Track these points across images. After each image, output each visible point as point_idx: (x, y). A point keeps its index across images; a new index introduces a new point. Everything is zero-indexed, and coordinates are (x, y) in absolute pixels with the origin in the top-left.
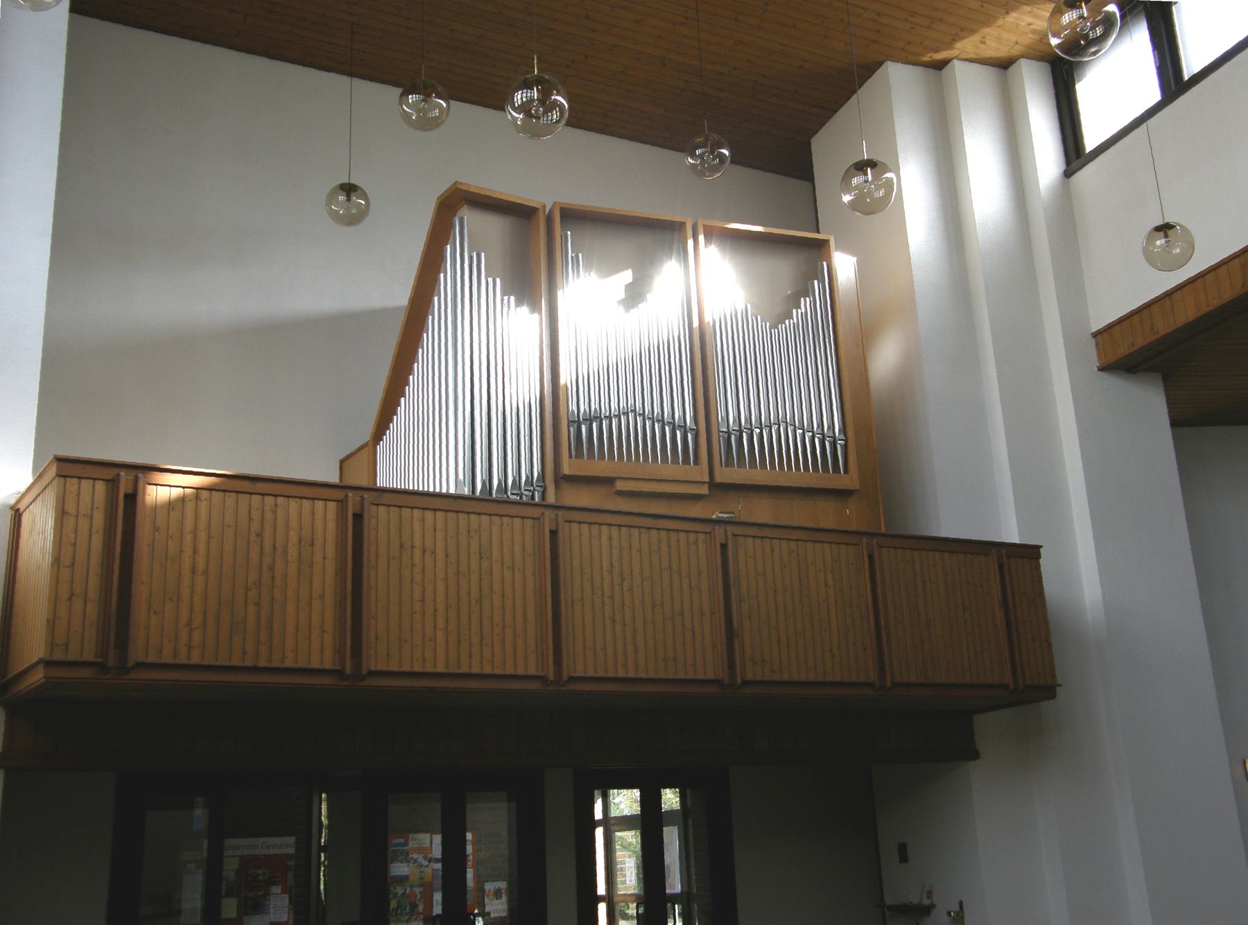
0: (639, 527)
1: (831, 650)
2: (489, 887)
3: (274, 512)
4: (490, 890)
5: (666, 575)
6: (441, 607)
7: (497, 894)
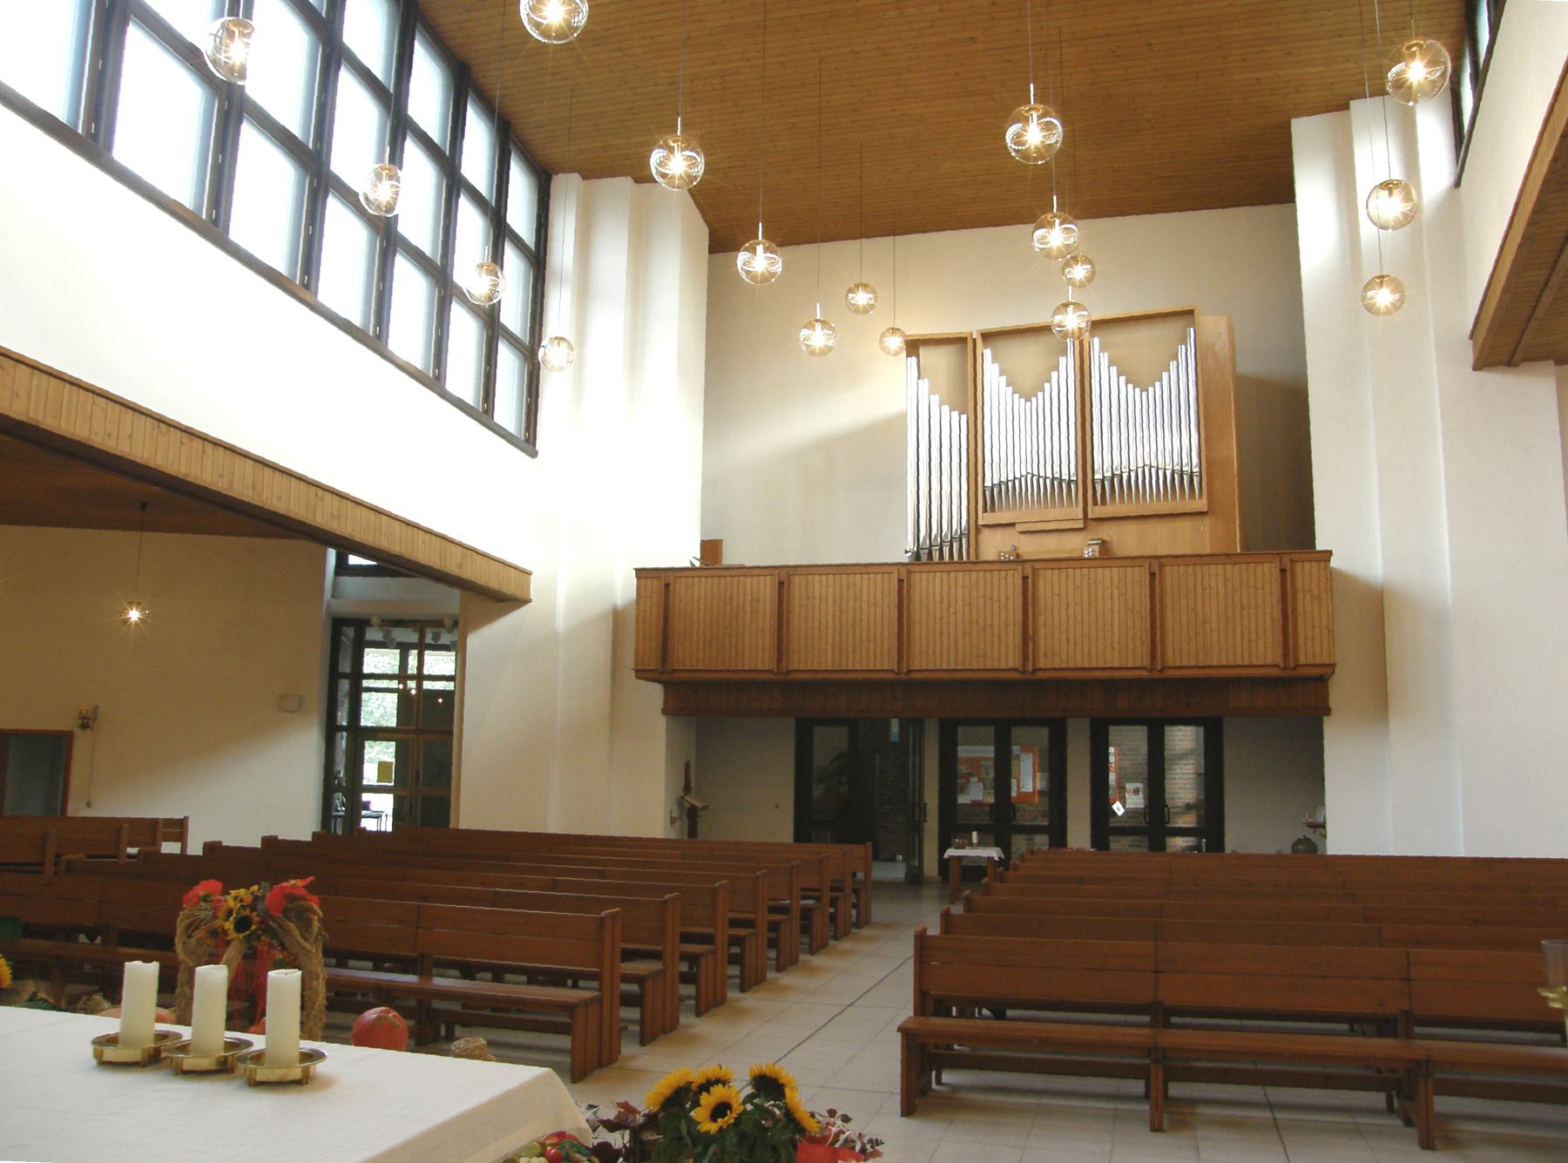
2: (1130, 786)
5: (982, 601)
6: (830, 632)
7: (1136, 791)
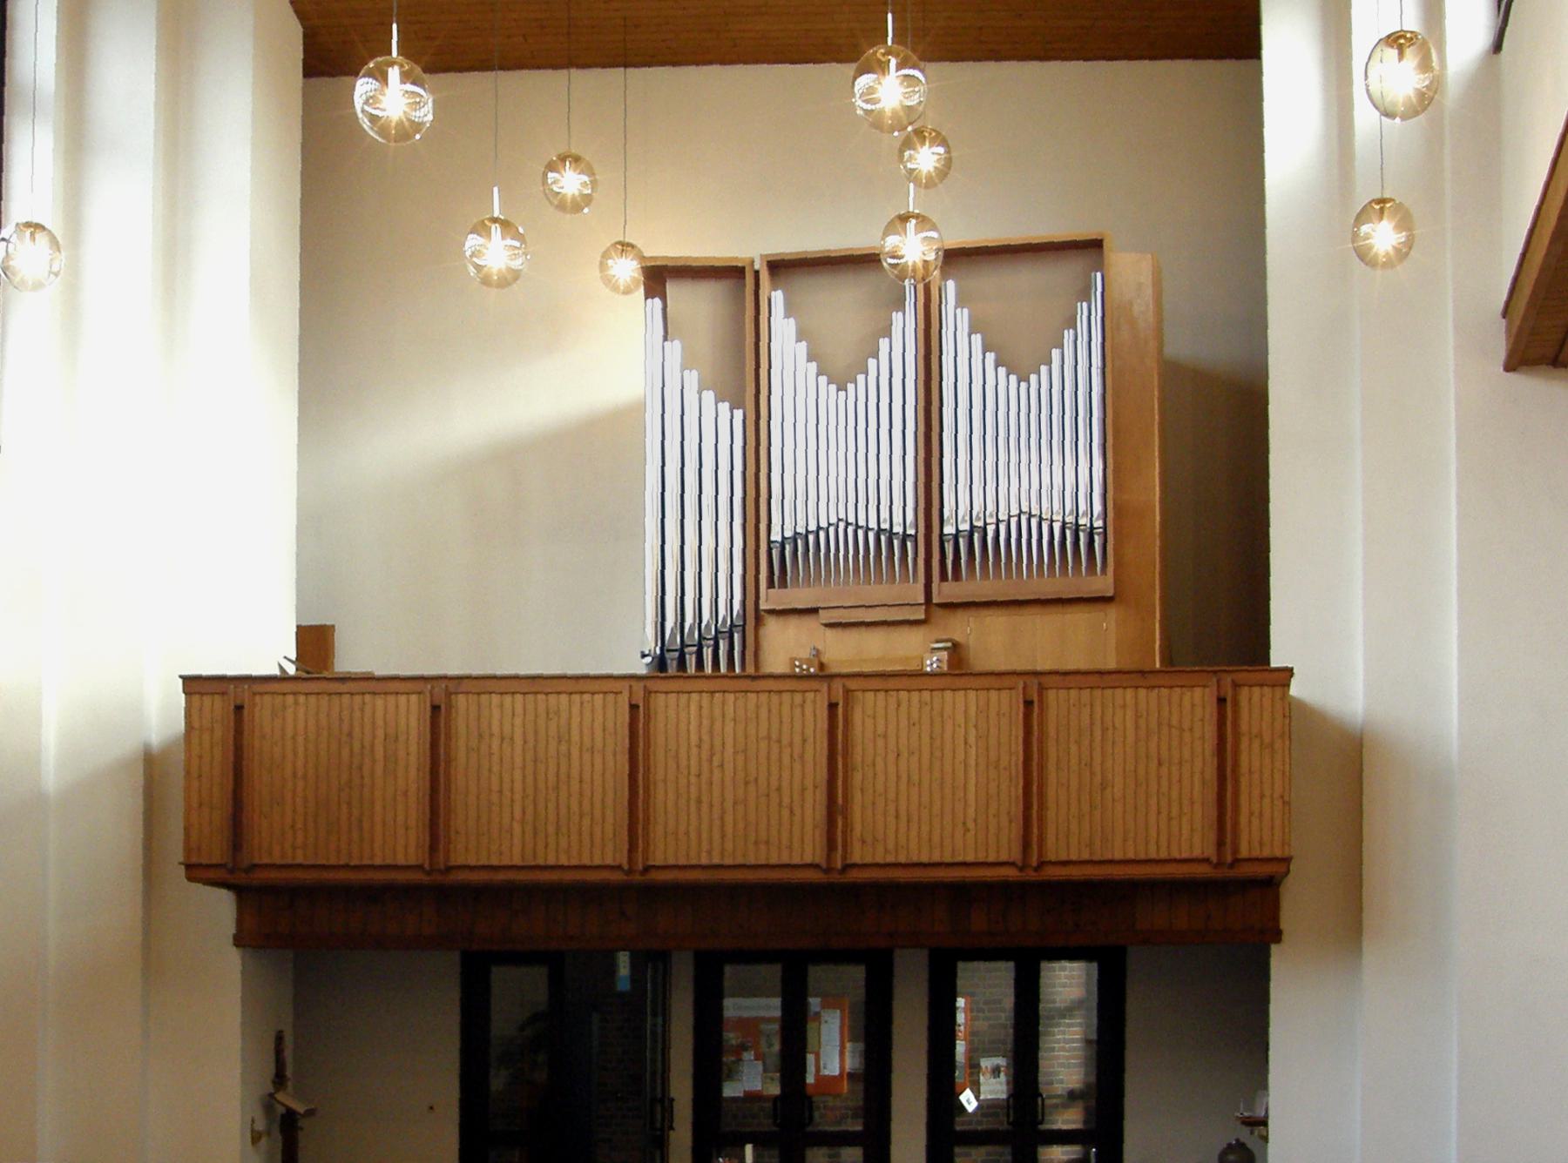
0: (735, 692)
1: (964, 823)
2: (986, 1063)
3: (362, 710)
4: (986, 1067)
5: (763, 745)
6: (518, 797)
7: (996, 1071)
